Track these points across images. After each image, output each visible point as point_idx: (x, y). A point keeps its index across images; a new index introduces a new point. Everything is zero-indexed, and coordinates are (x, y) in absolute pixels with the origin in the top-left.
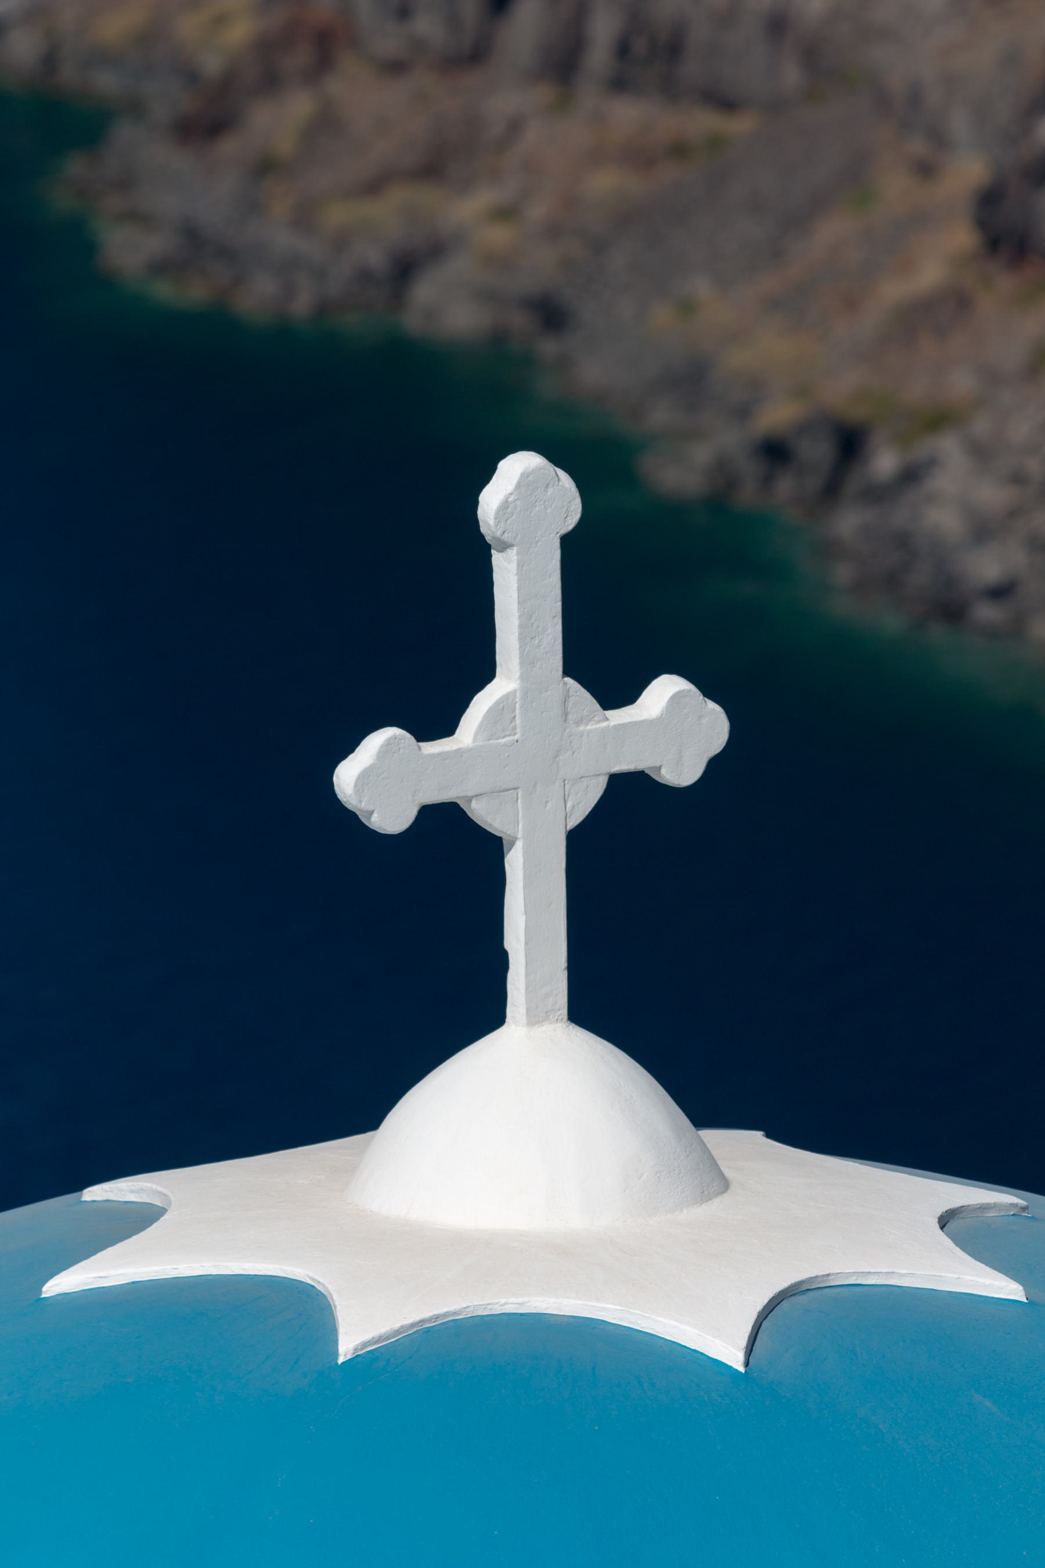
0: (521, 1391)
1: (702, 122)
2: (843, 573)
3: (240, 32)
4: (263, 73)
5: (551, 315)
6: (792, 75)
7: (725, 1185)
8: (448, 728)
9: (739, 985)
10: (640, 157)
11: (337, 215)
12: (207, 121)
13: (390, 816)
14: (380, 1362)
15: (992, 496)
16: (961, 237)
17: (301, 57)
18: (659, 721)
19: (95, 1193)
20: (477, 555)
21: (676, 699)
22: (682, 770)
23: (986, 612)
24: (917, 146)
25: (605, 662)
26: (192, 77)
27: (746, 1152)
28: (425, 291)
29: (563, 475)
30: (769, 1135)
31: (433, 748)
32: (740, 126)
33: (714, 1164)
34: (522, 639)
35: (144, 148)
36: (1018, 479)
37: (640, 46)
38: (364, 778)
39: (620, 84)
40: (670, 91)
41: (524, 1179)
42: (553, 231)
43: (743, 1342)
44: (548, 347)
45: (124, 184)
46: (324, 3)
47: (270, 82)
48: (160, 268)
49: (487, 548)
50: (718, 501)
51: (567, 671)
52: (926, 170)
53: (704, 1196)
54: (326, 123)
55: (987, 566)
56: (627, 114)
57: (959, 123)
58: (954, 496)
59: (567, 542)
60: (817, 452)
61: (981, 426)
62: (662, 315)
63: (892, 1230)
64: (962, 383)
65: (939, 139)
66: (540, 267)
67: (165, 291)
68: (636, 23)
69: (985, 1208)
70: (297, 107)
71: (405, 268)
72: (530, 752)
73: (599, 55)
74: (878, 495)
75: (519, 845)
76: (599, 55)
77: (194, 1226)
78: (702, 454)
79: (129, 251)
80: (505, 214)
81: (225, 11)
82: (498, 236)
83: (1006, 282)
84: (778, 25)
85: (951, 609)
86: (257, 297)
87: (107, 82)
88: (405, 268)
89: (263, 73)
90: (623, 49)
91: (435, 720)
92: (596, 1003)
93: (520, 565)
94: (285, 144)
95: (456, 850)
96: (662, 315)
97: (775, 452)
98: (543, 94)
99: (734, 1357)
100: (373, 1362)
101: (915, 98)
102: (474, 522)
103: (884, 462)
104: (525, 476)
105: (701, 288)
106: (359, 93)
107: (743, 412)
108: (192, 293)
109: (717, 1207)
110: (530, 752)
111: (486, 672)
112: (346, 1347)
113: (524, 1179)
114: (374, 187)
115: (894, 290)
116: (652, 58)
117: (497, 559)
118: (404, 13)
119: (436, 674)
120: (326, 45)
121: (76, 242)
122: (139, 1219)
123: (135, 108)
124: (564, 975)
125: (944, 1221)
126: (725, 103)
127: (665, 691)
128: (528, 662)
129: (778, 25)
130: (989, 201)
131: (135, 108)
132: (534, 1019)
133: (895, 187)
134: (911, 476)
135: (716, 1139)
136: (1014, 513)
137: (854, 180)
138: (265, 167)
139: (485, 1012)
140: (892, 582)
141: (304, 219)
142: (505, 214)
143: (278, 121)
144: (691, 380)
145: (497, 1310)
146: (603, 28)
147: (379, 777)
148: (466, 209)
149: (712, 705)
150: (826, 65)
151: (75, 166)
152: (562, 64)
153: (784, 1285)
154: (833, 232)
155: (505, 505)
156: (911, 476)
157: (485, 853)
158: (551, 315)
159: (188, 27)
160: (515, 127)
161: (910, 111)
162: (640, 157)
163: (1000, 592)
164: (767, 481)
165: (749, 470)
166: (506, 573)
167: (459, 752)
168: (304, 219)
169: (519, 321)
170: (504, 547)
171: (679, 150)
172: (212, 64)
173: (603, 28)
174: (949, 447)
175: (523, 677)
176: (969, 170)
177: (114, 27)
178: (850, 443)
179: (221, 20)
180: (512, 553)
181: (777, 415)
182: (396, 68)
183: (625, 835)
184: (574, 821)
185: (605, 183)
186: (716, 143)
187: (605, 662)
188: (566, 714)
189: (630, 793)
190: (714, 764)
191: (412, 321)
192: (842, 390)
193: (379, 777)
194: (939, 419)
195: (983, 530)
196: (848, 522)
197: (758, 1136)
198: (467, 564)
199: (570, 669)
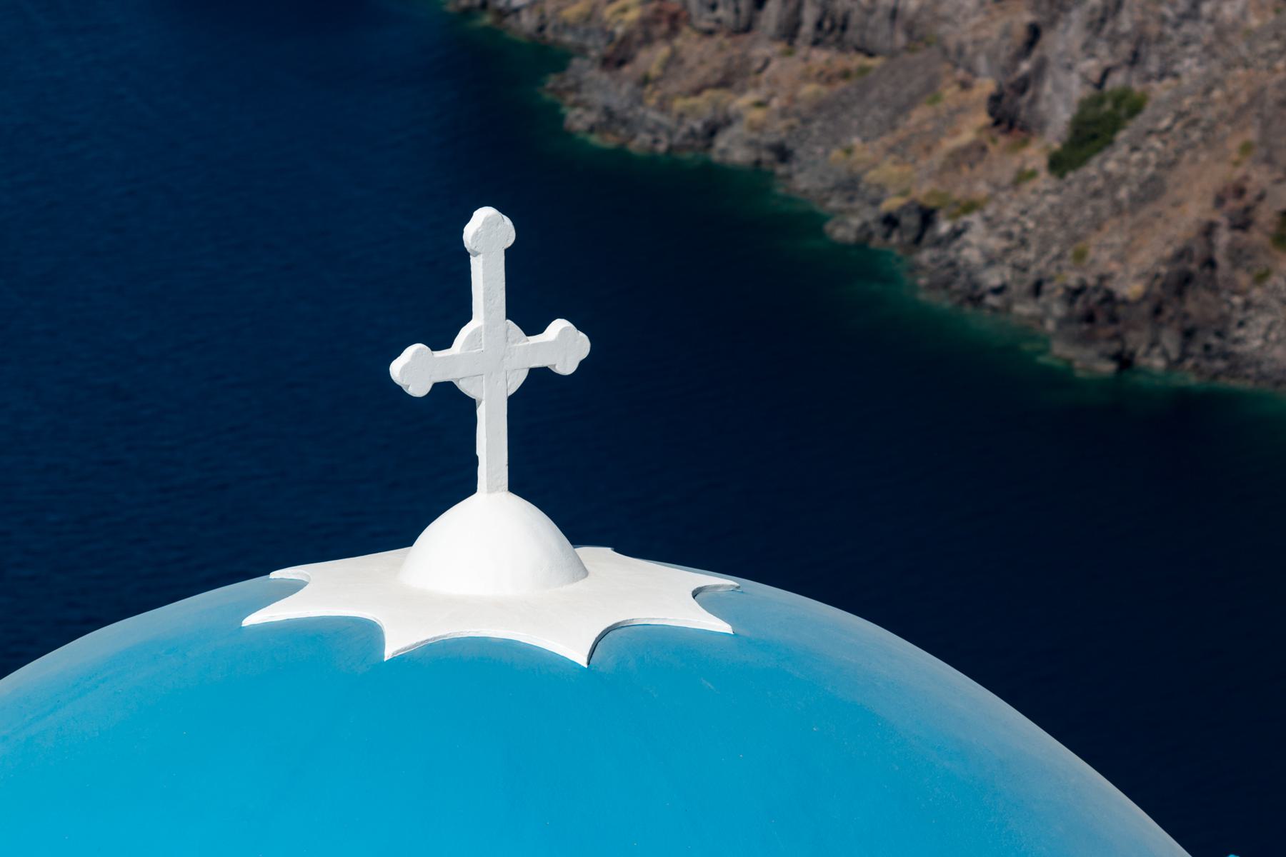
0: (479, 676)
1: (859, 60)
2: (923, 281)
3: (633, 15)
4: (646, 34)
5: (783, 153)
6: (901, 39)
7: (586, 573)
8: (448, 344)
9: (592, 473)
10: (826, 78)
11: (679, 104)
12: (616, 60)
13: (418, 388)
14: (406, 661)
15: (996, 244)
16: (983, 118)
17: (664, 27)
18: (554, 342)
19: (276, 575)
20: (463, 258)
21: (563, 331)
22: (566, 365)
23: (992, 300)
24: (961, 73)
25: (527, 313)
26: (610, 36)
27: (601, 558)
28: (721, 142)
29: (507, 219)
30: (616, 550)
31: (439, 354)
32: (875, 62)
33: (581, 563)
34: (485, 300)
35: (586, 70)
36: (1009, 236)
37: (827, 24)
38: (405, 369)
39: (816, 43)
40: (842, 46)
41: (488, 572)
42: (784, 113)
43: (587, 652)
44: (781, 170)
45: (576, 88)
46: (674, 3)
47: (648, 40)
48: (592, 129)
49: (468, 254)
50: (862, 245)
51: (508, 317)
52: (965, 86)
53: (575, 579)
54: (674, 60)
55: (993, 278)
56: (820, 57)
57: (982, 63)
58: (978, 243)
59: (508, 252)
60: (911, 221)
61: (990, 211)
62: (836, 153)
63: (669, 597)
64: (982, 189)
65: (971, 70)
66: (778, 130)
67: (595, 139)
68: (825, 13)
69: (717, 587)
70: (662, 51)
71: (712, 130)
72: (490, 357)
73: (807, 29)
74: (939, 242)
75: (483, 403)
76: (807, 29)
77: (319, 592)
78: (855, 222)
79: (578, 120)
80: (759, 104)
81: (627, 6)
82: (758, 114)
83: (1003, 140)
84: (894, 14)
85: (975, 298)
86: (640, 143)
87: (568, 38)
88: (712, 130)
89: (646, 34)
90: (819, 25)
91: (441, 340)
92: (518, 485)
93: (484, 263)
94: (654, 70)
95: (452, 406)
96: (836, 153)
97: (891, 221)
98: (780, 47)
99: (583, 662)
100: (402, 661)
101: (960, 51)
102: (461, 242)
103: (944, 227)
104: (487, 218)
105: (856, 141)
106: (689, 43)
107: (876, 203)
108: (607, 141)
109: (581, 585)
110: (490, 357)
111: (467, 317)
112: (389, 652)
113: (488, 572)
114: (697, 92)
115: (949, 144)
116: (833, 30)
117: (473, 260)
118: (713, 7)
119: (443, 319)
120: (675, 22)
121: (554, 115)
122: (294, 587)
123: (582, 51)
124: (506, 469)
125: (695, 594)
126: (871, 55)
127: (559, 327)
128: (488, 312)
129: (894, 14)
130: (995, 100)
131: (582, 51)
132: (491, 490)
133: (950, 93)
134: (957, 233)
135: (586, 552)
136: (1007, 251)
137: (930, 91)
138: (645, 81)
139: (465, 486)
140: (946, 285)
141: (663, 107)
142: (759, 104)
143: (652, 58)
144: (850, 186)
145: (466, 635)
146: (810, 15)
147: (414, 369)
148: (741, 102)
149: (581, 334)
150: (918, 34)
151: (552, 80)
152: (789, 32)
153: (610, 624)
154: (919, 114)
155: (476, 234)
156: (957, 233)
157: (468, 406)
158: (783, 153)
159: (608, 12)
160: (767, 62)
161: (958, 57)
162: (826, 78)
163: (998, 291)
164: (887, 236)
165: (878, 230)
166: (477, 267)
167: (453, 357)
168: (663, 107)
169: (767, 156)
170: (476, 254)
171: (846, 75)
172: (619, 30)
173: (810, 15)
174: (975, 218)
175: (486, 319)
176: (986, 86)
177: (572, 12)
178: (927, 217)
179: (624, 10)
180: (480, 258)
181: (892, 203)
182: (710, 33)
183: (536, 396)
184: (511, 392)
185: (808, 90)
186: (864, 71)
187: (527, 313)
188: (507, 338)
189: (540, 378)
190: (582, 363)
191: (715, 156)
192: (923, 191)
193: (414, 369)
194: (971, 207)
195: (991, 261)
196: (925, 256)
197: (609, 550)
198: (458, 264)
199: (509, 316)
